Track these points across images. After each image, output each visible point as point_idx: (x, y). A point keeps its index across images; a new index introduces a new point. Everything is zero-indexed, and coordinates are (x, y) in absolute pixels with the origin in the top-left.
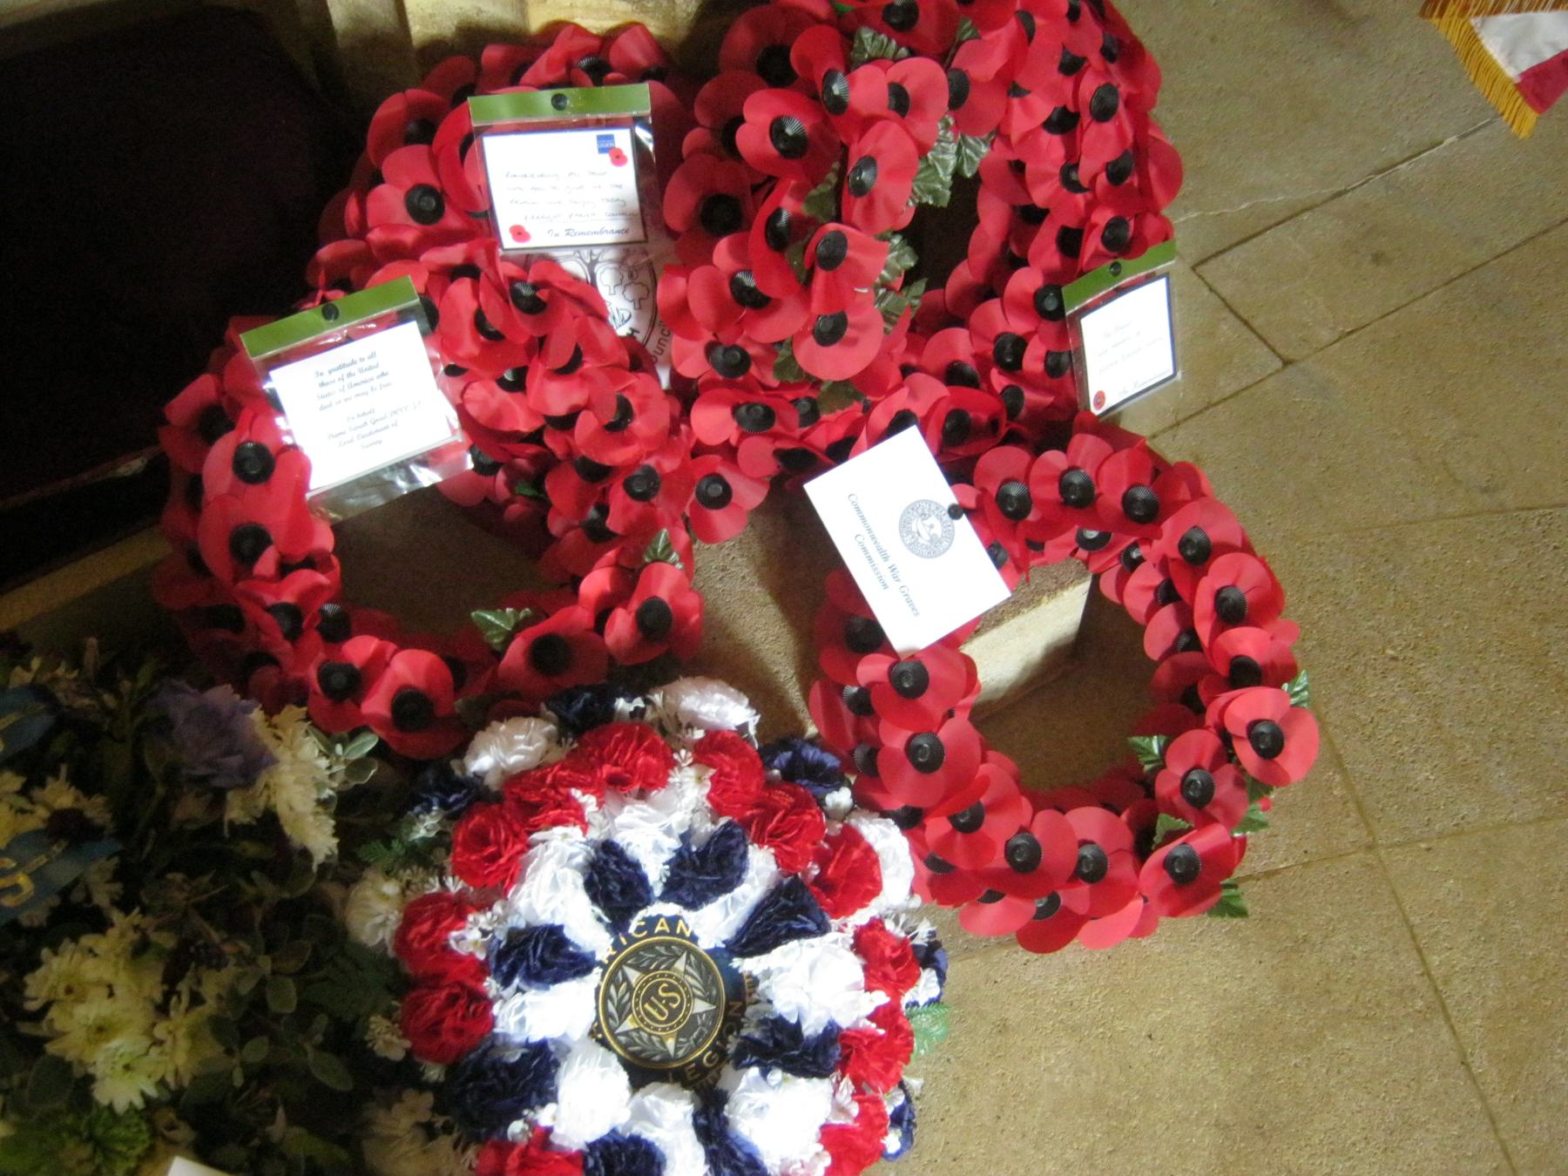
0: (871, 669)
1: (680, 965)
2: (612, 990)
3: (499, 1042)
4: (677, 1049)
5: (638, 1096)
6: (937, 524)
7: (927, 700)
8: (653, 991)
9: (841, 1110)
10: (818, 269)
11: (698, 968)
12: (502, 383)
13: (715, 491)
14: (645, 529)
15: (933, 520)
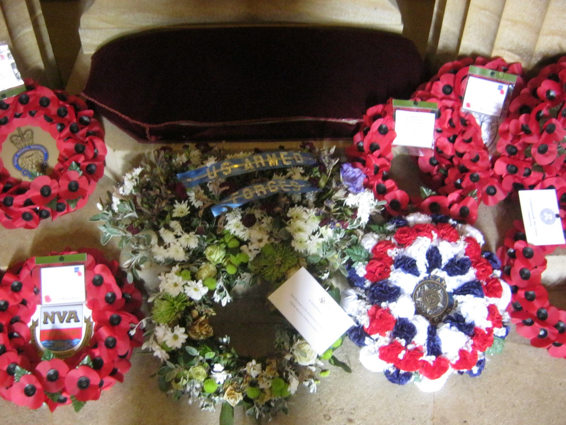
0: (519, 245)
1: (439, 291)
2: (419, 289)
3: (389, 282)
4: (430, 312)
5: (416, 316)
6: (551, 217)
7: (531, 261)
8: (430, 294)
9: (466, 346)
10: (545, 131)
11: (443, 295)
12: (449, 139)
13: (492, 191)
14: (471, 189)
15: (550, 215)
